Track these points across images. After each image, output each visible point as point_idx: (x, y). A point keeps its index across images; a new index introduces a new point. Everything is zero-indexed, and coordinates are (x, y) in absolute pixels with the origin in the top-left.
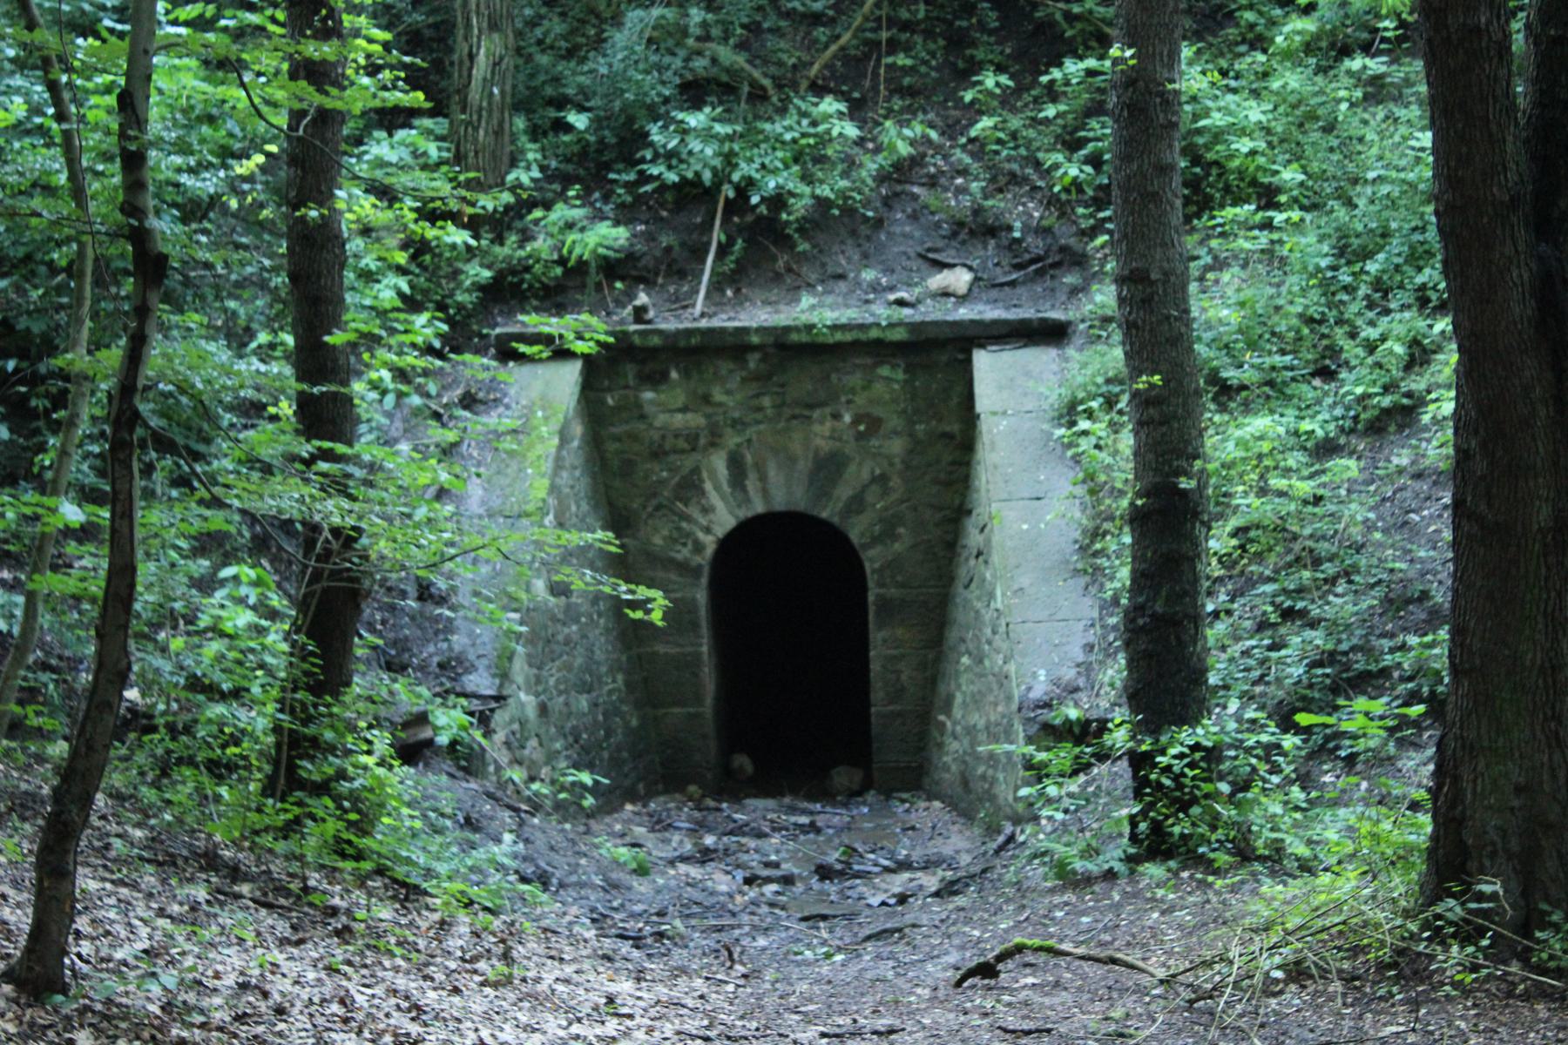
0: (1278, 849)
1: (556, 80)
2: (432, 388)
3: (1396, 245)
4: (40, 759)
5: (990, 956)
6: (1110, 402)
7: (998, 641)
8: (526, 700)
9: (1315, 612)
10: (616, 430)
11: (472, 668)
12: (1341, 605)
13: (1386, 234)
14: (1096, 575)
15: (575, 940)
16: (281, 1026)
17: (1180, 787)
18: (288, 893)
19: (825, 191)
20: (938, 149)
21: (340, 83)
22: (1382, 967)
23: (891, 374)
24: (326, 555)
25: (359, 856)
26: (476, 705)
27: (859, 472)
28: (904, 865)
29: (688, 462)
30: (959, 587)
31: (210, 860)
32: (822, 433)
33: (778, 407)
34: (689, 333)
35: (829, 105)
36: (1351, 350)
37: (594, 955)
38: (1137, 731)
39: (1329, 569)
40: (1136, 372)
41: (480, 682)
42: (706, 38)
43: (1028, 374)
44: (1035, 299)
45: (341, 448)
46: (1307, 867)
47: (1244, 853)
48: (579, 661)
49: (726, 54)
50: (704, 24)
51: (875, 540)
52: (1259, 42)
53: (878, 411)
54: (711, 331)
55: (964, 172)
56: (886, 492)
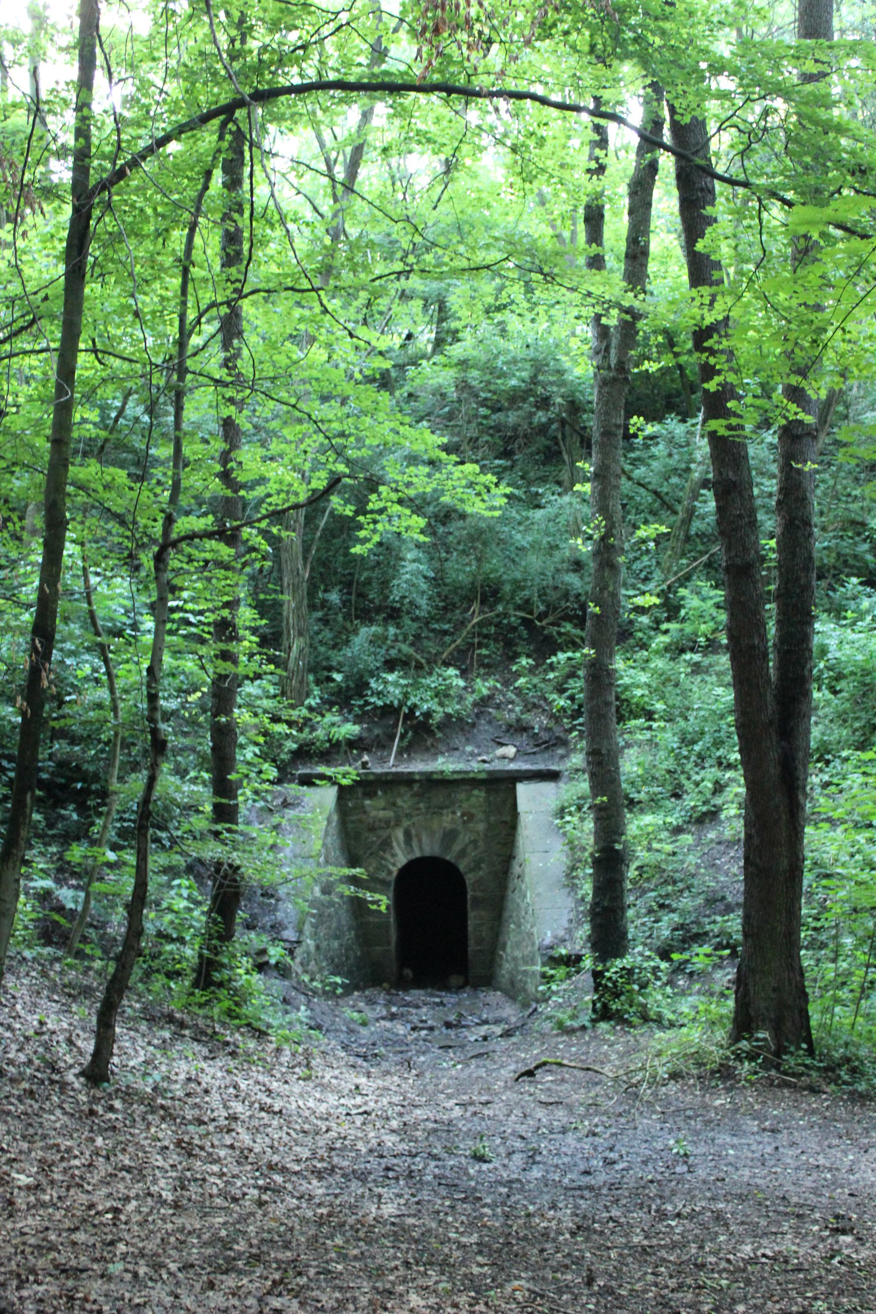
0: (660, 1016)
1: (328, 659)
2: (269, 798)
3: (708, 738)
4: (89, 968)
5: (532, 1067)
6: (579, 808)
7: (528, 917)
8: (310, 943)
9: (674, 905)
10: (354, 818)
11: (286, 928)
12: (686, 902)
13: (703, 733)
14: (573, 888)
15: (338, 1059)
16: (207, 1099)
17: (615, 986)
18: (206, 1035)
19: (449, 710)
20: (501, 691)
21: (235, 662)
22: (713, 1072)
23: (479, 794)
24: (225, 877)
25: (237, 1017)
26: (288, 945)
27: (463, 839)
28: (486, 1022)
29: (384, 834)
30: (509, 892)
31: (170, 1019)
32: (448, 820)
33: (428, 808)
34: (387, 774)
35: (452, 671)
36: (688, 785)
37: (347, 1065)
38: (596, 960)
39: (681, 885)
40: (595, 796)
41: (290, 934)
42: (396, 640)
43: (541, 794)
44: (544, 761)
45: (234, 827)
46: (672, 1025)
47: (645, 1018)
48: (334, 925)
49: (406, 648)
50: (396, 635)
51: (472, 870)
52: (644, 646)
53: (473, 811)
54: (397, 773)
55: (512, 702)
56: (476, 847)
